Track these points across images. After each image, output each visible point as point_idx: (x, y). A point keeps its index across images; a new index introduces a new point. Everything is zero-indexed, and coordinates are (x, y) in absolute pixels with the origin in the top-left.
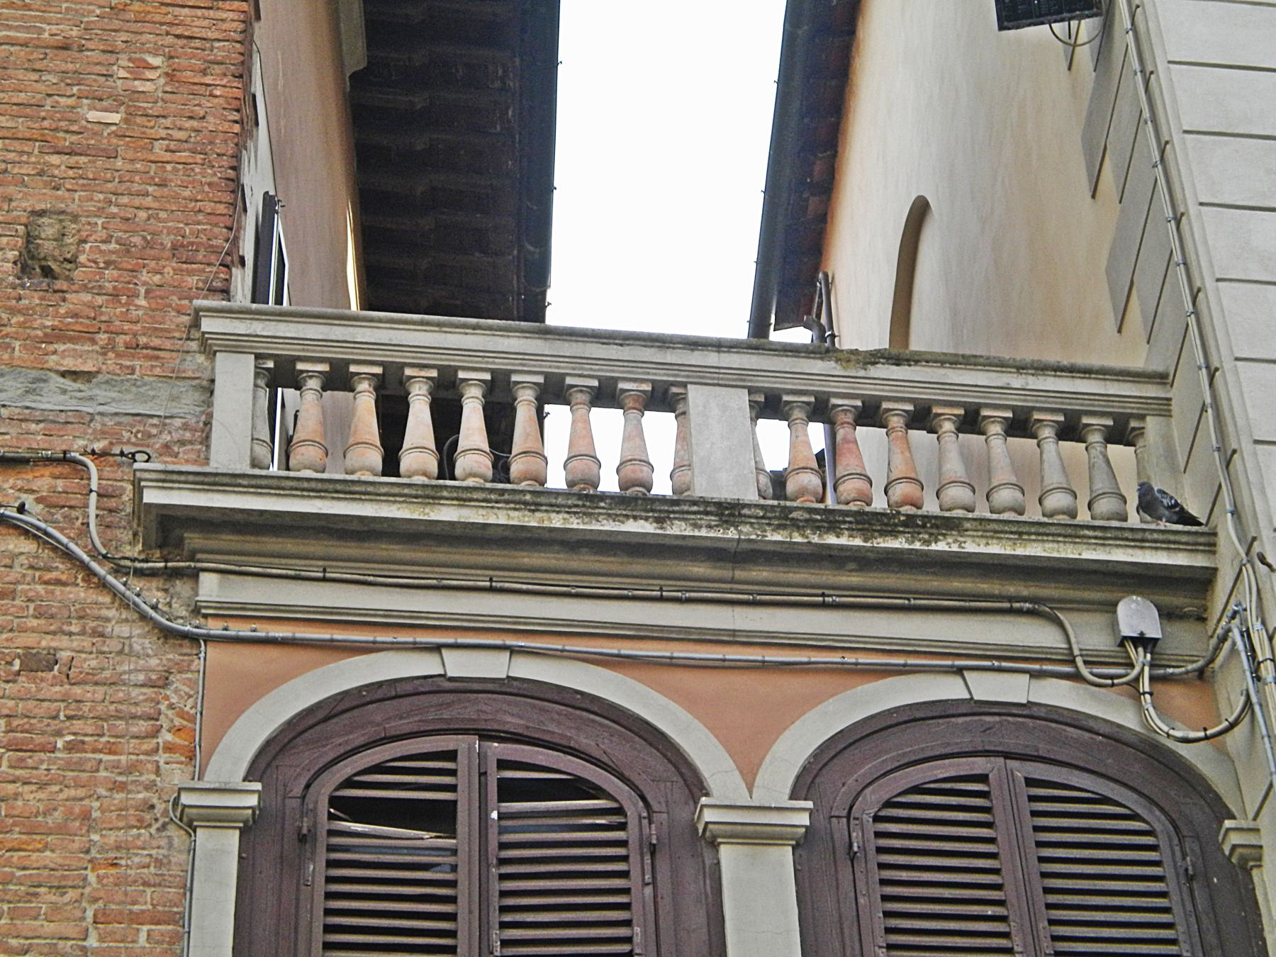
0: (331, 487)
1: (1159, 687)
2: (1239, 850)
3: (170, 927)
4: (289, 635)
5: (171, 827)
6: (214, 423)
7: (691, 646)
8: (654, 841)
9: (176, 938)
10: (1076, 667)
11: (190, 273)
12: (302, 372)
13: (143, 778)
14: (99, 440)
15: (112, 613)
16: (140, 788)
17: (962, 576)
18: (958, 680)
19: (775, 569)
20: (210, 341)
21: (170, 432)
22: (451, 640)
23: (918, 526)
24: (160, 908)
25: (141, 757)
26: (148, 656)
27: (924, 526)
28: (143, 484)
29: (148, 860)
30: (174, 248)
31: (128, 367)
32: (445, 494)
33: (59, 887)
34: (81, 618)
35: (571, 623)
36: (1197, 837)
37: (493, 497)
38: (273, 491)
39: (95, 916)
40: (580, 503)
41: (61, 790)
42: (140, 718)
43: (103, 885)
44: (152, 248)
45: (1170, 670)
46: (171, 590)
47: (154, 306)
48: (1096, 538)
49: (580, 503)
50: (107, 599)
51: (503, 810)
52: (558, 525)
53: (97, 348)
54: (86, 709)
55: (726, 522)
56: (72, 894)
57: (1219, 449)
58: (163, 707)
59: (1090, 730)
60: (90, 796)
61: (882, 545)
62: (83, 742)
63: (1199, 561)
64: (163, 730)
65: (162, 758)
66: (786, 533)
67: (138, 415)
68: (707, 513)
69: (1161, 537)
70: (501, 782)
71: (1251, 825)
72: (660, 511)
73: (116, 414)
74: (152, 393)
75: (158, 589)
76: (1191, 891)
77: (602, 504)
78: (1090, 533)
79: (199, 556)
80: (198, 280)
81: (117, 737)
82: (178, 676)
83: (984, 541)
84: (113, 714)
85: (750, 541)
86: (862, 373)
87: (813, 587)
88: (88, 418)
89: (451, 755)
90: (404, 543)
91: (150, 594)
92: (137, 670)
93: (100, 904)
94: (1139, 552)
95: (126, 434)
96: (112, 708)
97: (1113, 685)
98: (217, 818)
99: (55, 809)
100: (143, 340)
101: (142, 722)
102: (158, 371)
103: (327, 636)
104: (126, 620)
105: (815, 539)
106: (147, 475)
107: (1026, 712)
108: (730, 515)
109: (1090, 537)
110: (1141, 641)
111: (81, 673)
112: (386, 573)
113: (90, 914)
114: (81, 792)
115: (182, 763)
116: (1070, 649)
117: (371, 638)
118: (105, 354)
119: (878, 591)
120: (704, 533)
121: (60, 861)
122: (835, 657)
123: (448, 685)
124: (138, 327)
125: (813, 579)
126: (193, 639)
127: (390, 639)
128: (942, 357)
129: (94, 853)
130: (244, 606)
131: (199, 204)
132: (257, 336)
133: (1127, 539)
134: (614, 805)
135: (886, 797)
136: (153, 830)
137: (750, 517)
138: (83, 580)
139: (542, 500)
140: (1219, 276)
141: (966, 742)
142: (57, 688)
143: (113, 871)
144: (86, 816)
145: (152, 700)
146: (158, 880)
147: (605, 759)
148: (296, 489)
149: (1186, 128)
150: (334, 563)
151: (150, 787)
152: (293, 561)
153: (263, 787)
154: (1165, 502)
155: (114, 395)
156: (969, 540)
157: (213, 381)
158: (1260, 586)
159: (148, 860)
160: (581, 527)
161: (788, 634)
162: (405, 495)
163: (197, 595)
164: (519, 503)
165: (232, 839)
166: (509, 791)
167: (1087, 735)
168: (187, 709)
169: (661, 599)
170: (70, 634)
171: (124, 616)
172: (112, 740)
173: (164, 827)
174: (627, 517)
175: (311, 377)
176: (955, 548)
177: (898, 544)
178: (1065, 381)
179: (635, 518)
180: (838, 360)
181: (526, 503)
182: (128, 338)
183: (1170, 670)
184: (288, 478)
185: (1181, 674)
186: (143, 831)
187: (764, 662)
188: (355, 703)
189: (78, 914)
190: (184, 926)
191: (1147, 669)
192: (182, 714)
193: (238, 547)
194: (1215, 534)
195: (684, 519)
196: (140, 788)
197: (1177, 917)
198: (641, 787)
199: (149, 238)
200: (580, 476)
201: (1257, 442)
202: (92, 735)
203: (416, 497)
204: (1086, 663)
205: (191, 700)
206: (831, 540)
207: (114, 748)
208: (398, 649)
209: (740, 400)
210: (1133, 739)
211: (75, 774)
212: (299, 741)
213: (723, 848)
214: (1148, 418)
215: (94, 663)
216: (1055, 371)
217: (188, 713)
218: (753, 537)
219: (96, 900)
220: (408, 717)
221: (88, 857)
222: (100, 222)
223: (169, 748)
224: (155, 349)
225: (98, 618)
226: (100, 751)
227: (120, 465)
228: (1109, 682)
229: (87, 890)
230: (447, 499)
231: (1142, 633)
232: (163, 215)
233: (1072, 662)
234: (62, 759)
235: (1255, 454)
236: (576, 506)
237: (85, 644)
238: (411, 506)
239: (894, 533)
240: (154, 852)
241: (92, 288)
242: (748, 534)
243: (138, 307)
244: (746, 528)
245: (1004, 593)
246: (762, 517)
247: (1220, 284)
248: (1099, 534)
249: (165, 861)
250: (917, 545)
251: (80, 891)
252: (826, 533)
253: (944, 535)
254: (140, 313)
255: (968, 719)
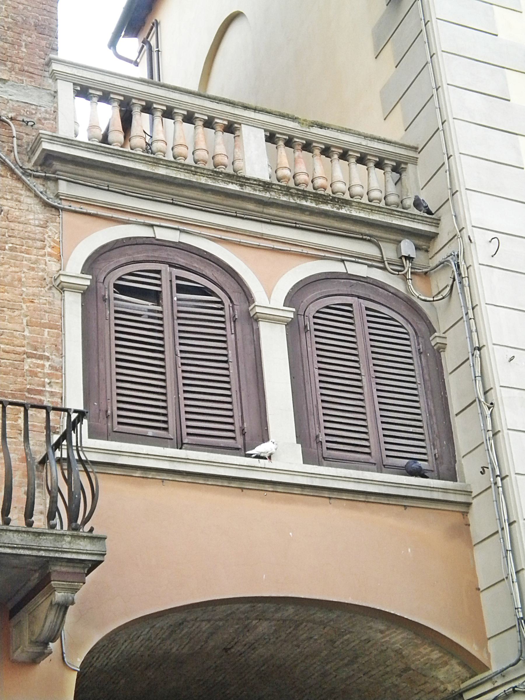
0: (117, 153)
1: (413, 276)
2: (438, 345)
3: (56, 331)
4: (95, 212)
5: (53, 288)
6: (59, 113)
7: (245, 237)
8: (237, 317)
9: (58, 336)
10: (385, 265)
11: (43, 39)
12: (91, 94)
13: (41, 266)
14: (11, 112)
15: (23, 192)
16: (39, 270)
17: (348, 223)
18: (342, 264)
19: (279, 210)
20: (56, 74)
21: (40, 114)
22: (158, 223)
23: (336, 201)
24: (51, 322)
25: (39, 257)
26: (38, 213)
27: (338, 202)
28: (42, 139)
29: (45, 301)
30: (35, 26)
31: (20, 80)
32: (161, 162)
33: (11, 309)
34: (11, 192)
35: (209, 223)
36: (423, 337)
37: (180, 166)
38: (94, 151)
39: (27, 322)
40: (212, 174)
41: (9, 268)
42: (38, 240)
43: (29, 310)
44: (26, 24)
45: (416, 270)
46: (46, 185)
47: (29, 52)
48: (398, 215)
49: (212, 174)
50: (20, 186)
51: (179, 297)
52: (204, 182)
53: (7, 68)
54: (16, 233)
55: (266, 190)
56: (17, 313)
57: (450, 189)
58: (46, 236)
59: (387, 290)
60: (21, 271)
61: (322, 208)
62: (16, 248)
63: (433, 230)
64: (47, 247)
65: (47, 258)
66: (287, 197)
67: (27, 103)
68: (259, 185)
69: (421, 218)
70: (177, 285)
71: (444, 335)
72: (242, 182)
73: (17, 101)
74: (31, 93)
75: (41, 184)
76: (420, 357)
77: (221, 176)
78: (397, 213)
79: (58, 173)
80: (46, 43)
81: (29, 247)
82: (51, 224)
83: (358, 211)
84: (27, 237)
85: (274, 199)
86: (308, 130)
87: (293, 219)
88: (6, 102)
89: (159, 272)
90: (140, 179)
91: (38, 186)
92: (35, 219)
93: (28, 318)
94: (412, 223)
95: (22, 111)
96: (26, 234)
97: (398, 274)
98: (73, 288)
99: (7, 275)
100: (26, 68)
101: (38, 242)
102: (33, 84)
103: (110, 215)
104: (29, 196)
105: (298, 202)
106: (44, 136)
107: (366, 281)
108: (268, 187)
109: (396, 215)
110: (409, 258)
111: (13, 217)
112: (133, 191)
113: (25, 321)
114: (17, 269)
115: (55, 262)
116: (383, 257)
117: (127, 218)
118: (11, 72)
119: (315, 224)
120: (257, 193)
121: (12, 298)
122: (299, 250)
123: (157, 242)
124: (23, 61)
125: (292, 216)
126: (57, 208)
127: (135, 220)
128: (338, 128)
129: (24, 296)
130: (77, 197)
131: (44, 6)
132: (75, 75)
133: (409, 218)
134: (220, 300)
135: (317, 309)
136: (46, 289)
137: (275, 189)
138: (10, 176)
139: (198, 170)
140: (454, 117)
141: (344, 290)
142: (4, 223)
143: (32, 304)
144: (20, 280)
145: (42, 233)
146: (50, 310)
147: (215, 280)
148: (103, 151)
149: (443, 50)
150: (112, 184)
151: (44, 270)
152: (95, 180)
153: (93, 277)
154: (424, 204)
155: (15, 92)
156: (353, 210)
157: (56, 92)
158: (465, 247)
159: (45, 301)
160: (212, 184)
161: (275, 237)
162: (146, 161)
163: (58, 190)
164: (188, 170)
165: (78, 298)
166: (181, 289)
167: (386, 292)
168: (55, 238)
169: (236, 217)
170: (7, 199)
171: (28, 194)
172: (27, 248)
173: (50, 288)
174: (229, 182)
175: (94, 97)
176: (348, 213)
177: (327, 207)
178: (382, 145)
179: (232, 183)
180: (299, 123)
181: (192, 171)
182: (20, 66)
183: (416, 270)
184: (101, 146)
185: (420, 272)
186: (42, 289)
187: (273, 248)
188: (120, 245)
189: (21, 321)
190: (62, 331)
191: (410, 269)
192: (54, 241)
193: (75, 171)
194: (440, 220)
195: (251, 186)
196: (39, 270)
197: (416, 367)
198: (230, 294)
199: (24, 18)
200: (202, 158)
201: (467, 189)
202: (19, 245)
203: (150, 162)
204: (388, 263)
205: (57, 235)
206: (304, 203)
207: (28, 251)
208: (136, 224)
209: (261, 135)
210: (401, 296)
211: (14, 261)
212: (100, 258)
213: (260, 322)
214: (409, 164)
215: (17, 213)
216: (378, 140)
217: (56, 240)
218: (276, 197)
219: (27, 316)
220: (141, 253)
221: (22, 297)
222: (4, 7)
223: (50, 255)
224: (31, 73)
225: (17, 194)
226: (22, 252)
227: (21, 125)
228: (397, 273)
229: (23, 311)
230: (162, 164)
231: (409, 255)
232: (29, 8)
233: (383, 262)
234: (9, 254)
235: (466, 194)
236: (211, 175)
237: (13, 204)
238: (148, 165)
239: (326, 203)
240: (48, 298)
241: (3, 39)
242: (273, 196)
243: (23, 52)
244: (273, 193)
245: (360, 232)
246: (280, 190)
247: (455, 120)
248: (400, 214)
249: (52, 303)
250: (335, 210)
251: (20, 311)
252: (302, 199)
253: (345, 207)
254: (24, 54)
255: (345, 280)
